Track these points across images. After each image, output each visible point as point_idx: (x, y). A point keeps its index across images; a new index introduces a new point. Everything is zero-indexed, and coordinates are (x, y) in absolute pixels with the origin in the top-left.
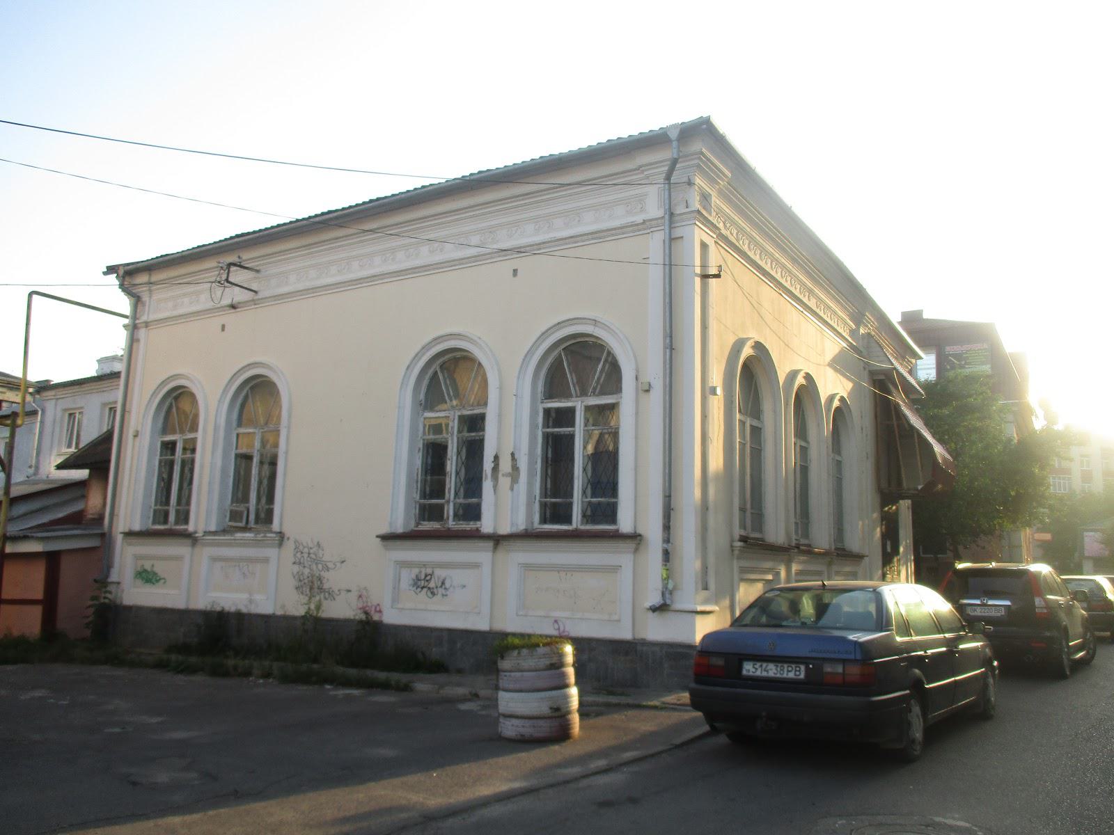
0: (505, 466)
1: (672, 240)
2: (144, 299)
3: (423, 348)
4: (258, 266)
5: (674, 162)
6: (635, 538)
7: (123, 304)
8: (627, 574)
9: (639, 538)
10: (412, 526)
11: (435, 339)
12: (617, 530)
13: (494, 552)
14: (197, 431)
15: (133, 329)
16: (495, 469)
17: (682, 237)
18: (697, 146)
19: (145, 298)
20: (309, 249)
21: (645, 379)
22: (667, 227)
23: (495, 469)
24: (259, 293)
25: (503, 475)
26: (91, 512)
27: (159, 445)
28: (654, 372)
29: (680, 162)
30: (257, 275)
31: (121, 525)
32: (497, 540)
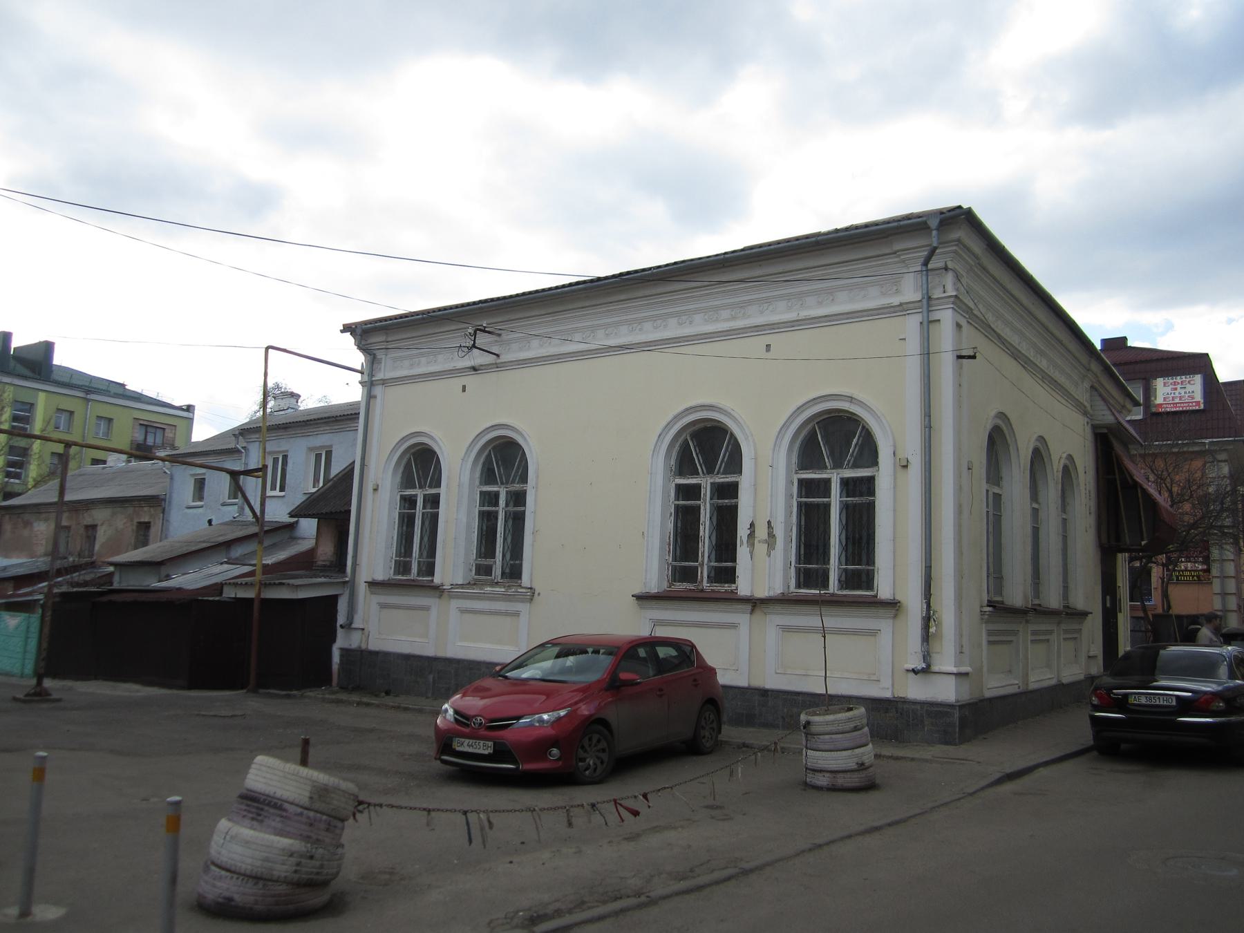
0: (761, 533)
6: (893, 606)
7: (357, 359)
8: (885, 638)
11: (687, 410)
13: (751, 614)
16: (751, 535)
17: (939, 320)
19: (380, 354)
20: (554, 316)
23: (751, 535)
25: (759, 542)
26: (321, 558)
27: (398, 498)
31: (364, 575)
32: (755, 604)
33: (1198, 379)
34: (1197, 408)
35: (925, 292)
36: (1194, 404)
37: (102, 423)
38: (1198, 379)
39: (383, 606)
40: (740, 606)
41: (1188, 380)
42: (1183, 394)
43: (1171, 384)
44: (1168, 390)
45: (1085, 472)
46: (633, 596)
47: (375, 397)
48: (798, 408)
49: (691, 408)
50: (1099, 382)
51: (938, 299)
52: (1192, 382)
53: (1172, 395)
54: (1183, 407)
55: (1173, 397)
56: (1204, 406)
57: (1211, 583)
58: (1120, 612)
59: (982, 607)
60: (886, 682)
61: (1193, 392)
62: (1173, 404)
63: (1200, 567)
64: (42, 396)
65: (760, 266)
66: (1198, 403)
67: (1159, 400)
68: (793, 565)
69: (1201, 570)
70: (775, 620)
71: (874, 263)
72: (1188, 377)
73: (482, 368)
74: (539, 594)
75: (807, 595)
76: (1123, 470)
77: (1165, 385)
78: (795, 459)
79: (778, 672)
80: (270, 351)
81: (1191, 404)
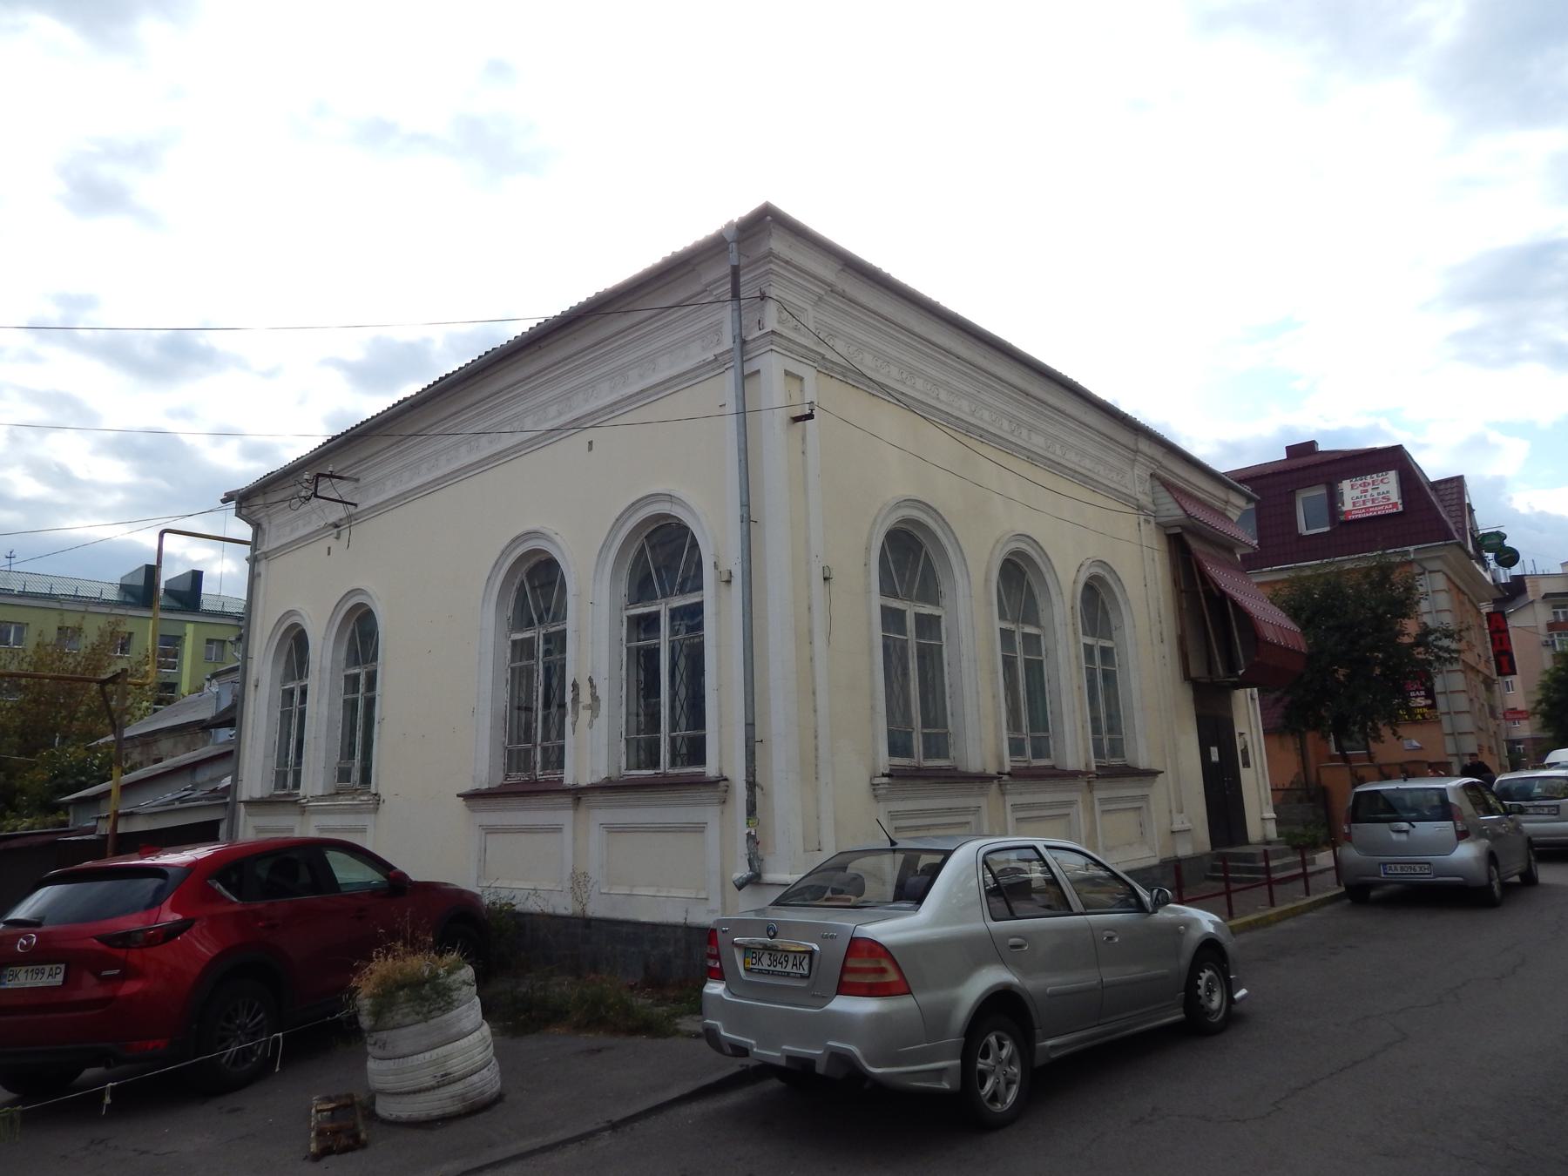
0: (585, 697)
1: (745, 378)
2: (264, 527)
3: (503, 553)
4: (356, 474)
5: (736, 272)
7: (244, 531)
8: (713, 833)
9: (722, 784)
10: (498, 780)
11: (513, 541)
12: (1053, 767)
14: (700, 588)
15: (253, 561)
16: (576, 700)
17: (758, 371)
18: (778, 244)
19: (265, 525)
21: (723, 567)
22: (738, 364)
24: (359, 506)
28: (733, 563)
29: (744, 275)
30: (356, 485)
32: (578, 794)
33: (1392, 476)
34: (1395, 510)
35: (737, 331)
36: (1391, 506)
37: (215, 647)
38: (1392, 476)
39: (490, 830)
40: (561, 800)
41: (1380, 479)
42: (1376, 496)
43: (1360, 485)
44: (1357, 493)
45: (1146, 586)
46: (458, 796)
47: (259, 575)
48: (617, 520)
49: (518, 538)
50: (1161, 466)
51: (754, 340)
52: (1385, 481)
53: (1363, 498)
54: (1377, 511)
55: (1364, 501)
56: (1403, 507)
57: (1440, 721)
58: (1246, 764)
59: (873, 777)
60: (715, 903)
61: (1388, 492)
62: (1365, 508)
63: (1423, 703)
64: (190, 628)
65: (575, 339)
66: (1395, 505)
67: (1348, 506)
68: (623, 737)
69: (1425, 706)
70: (601, 814)
71: (984, 379)
72: (1380, 474)
73: (342, 523)
74: (384, 801)
75: (639, 778)
76: (1206, 579)
77: (1352, 488)
78: (623, 588)
79: (603, 891)
80: (166, 535)
81: (1386, 507)
